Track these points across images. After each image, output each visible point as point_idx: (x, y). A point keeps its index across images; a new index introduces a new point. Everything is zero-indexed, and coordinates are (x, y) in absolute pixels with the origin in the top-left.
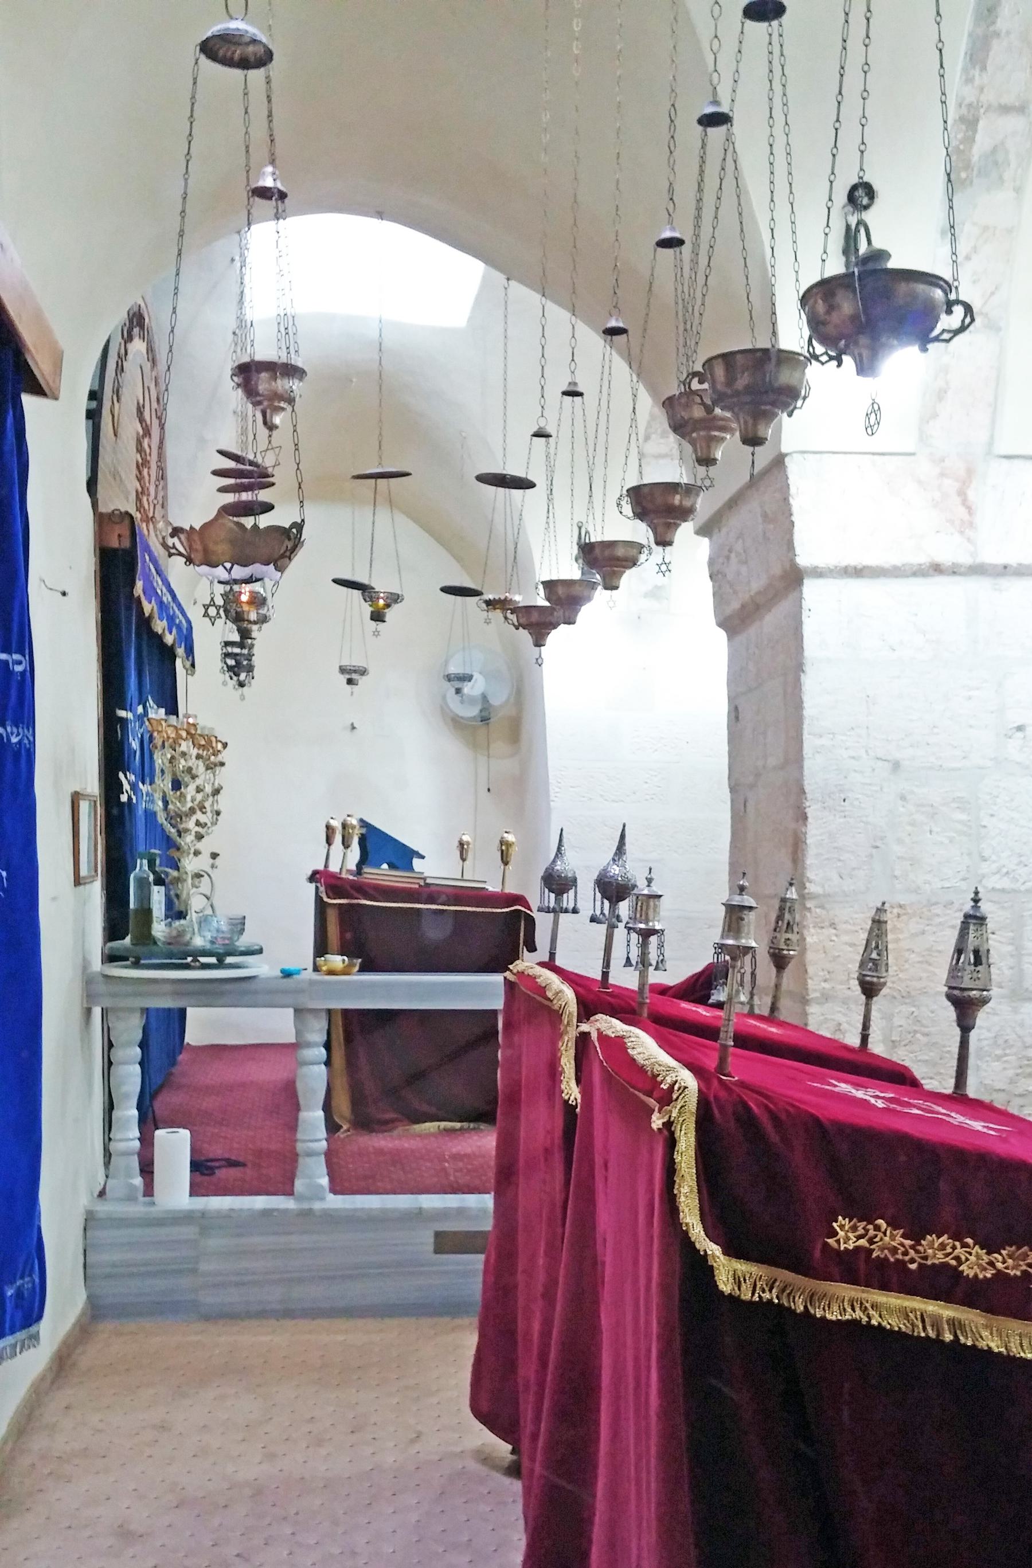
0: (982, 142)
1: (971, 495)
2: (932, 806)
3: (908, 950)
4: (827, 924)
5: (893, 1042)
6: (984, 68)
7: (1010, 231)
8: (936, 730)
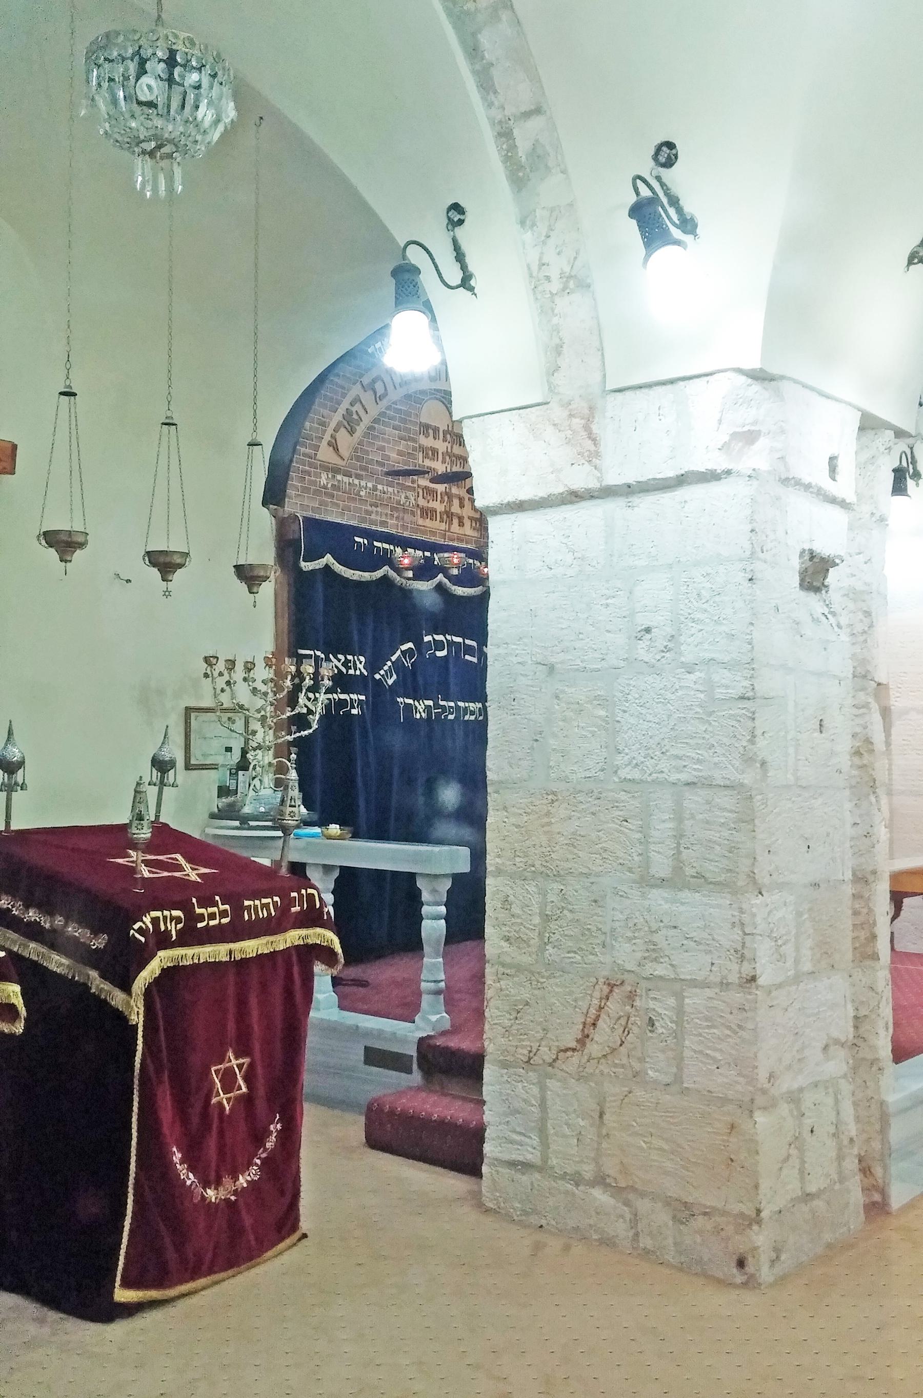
0: (523, 146)
1: (595, 428)
2: (578, 703)
3: (559, 833)
4: (501, 807)
5: (547, 915)
6: (495, 92)
7: (571, 205)
8: (581, 636)
